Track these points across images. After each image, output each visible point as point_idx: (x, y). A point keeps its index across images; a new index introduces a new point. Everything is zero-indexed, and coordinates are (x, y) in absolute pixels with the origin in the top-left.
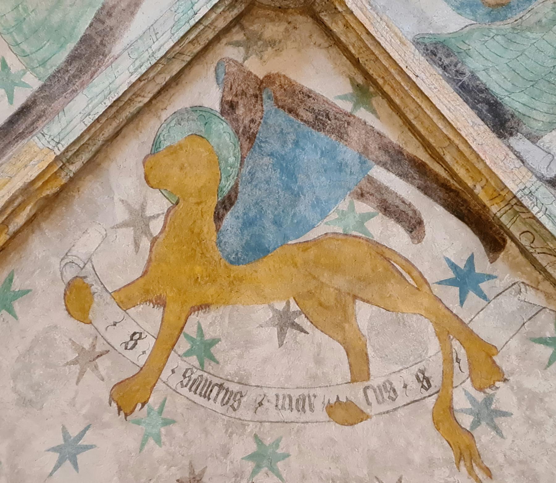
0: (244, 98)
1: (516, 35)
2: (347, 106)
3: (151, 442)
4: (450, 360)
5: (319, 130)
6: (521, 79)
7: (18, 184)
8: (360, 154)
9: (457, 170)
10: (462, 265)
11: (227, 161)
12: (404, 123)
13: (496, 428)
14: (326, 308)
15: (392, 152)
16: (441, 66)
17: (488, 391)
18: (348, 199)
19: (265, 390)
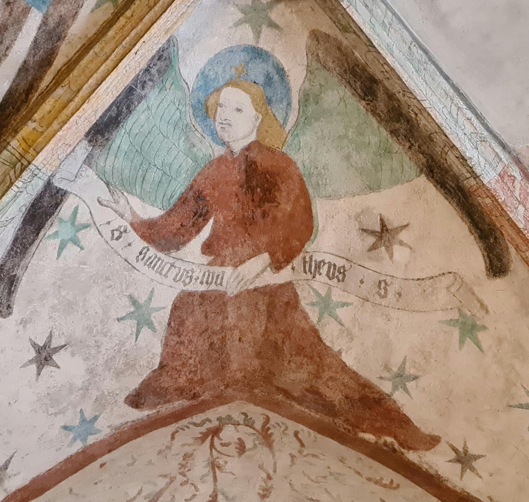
1: (181, 128)
6: (142, 140)
9: (49, 102)
12: (90, 38)
15: (58, 30)
16: (149, 66)
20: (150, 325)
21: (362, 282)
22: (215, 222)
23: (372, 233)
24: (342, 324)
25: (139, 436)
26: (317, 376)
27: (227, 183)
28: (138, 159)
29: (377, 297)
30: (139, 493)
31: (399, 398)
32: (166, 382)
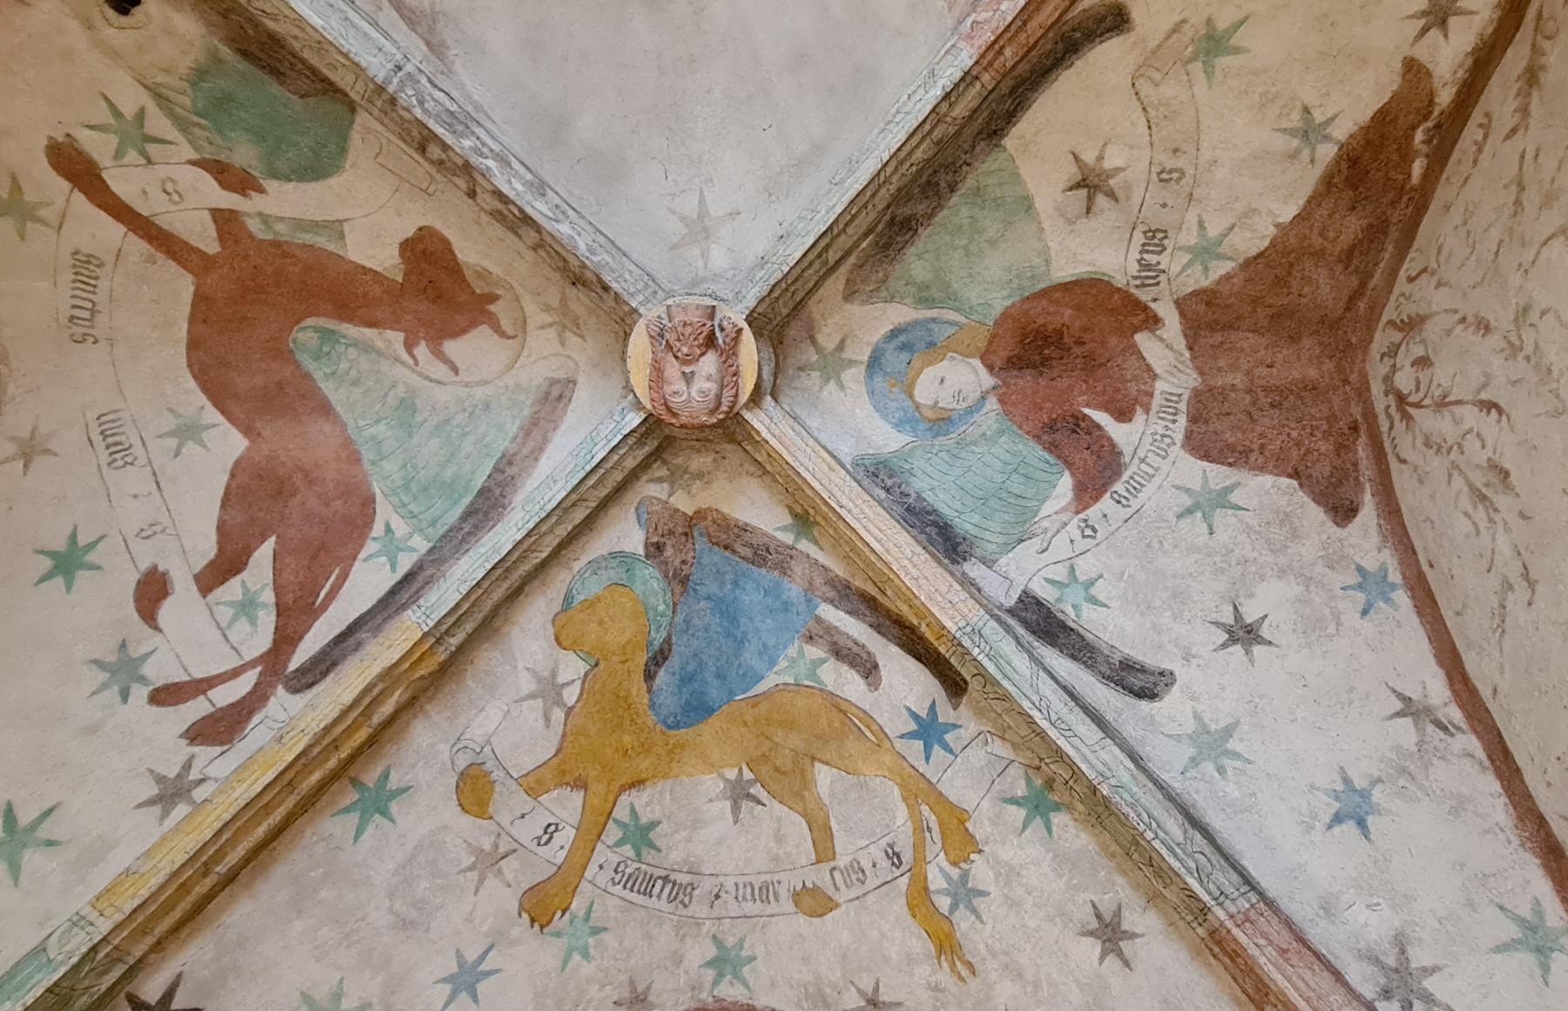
0: (672, 540)
2: (788, 538)
3: (577, 957)
4: (920, 829)
5: (760, 566)
7: (376, 669)
8: (806, 591)
10: (923, 714)
11: (655, 610)
13: (974, 911)
14: (784, 773)
17: (963, 865)
18: (797, 643)
19: (722, 879)
20: (1229, 490)
21: (1164, 205)
22: (1088, 406)
23: (1090, 199)
24: (1232, 228)
25: (1399, 510)
26: (1319, 254)
27: (1035, 393)
28: (993, 502)
29: (1184, 182)
30: (1467, 514)
31: (1343, 130)
32: (1322, 469)
